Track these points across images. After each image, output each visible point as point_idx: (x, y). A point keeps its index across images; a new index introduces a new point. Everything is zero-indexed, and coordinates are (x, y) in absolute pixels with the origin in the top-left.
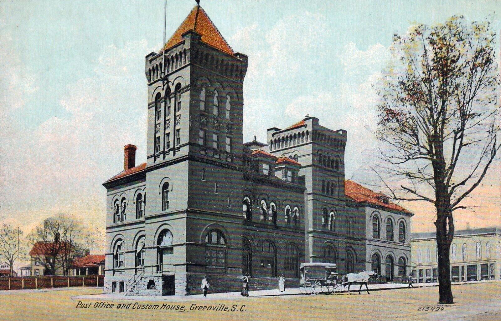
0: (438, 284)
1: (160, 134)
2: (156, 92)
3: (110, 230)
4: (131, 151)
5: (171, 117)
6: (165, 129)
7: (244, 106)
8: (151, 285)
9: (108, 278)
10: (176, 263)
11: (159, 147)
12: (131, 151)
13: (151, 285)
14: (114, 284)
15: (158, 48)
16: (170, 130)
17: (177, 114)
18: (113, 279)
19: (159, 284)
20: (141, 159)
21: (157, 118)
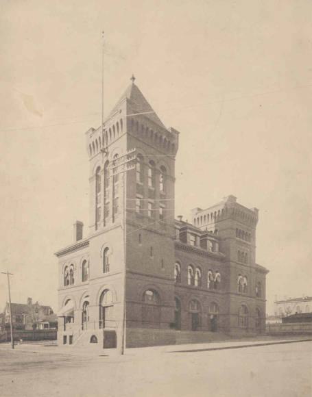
0: (267, 322)
1: (101, 205)
2: (97, 166)
3: (61, 292)
4: (79, 226)
5: (110, 188)
6: (105, 199)
7: (179, 157)
8: (93, 339)
9: (61, 333)
10: (117, 320)
11: (102, 215)
12: (79, 226)
13: (93, 339)
14: (65, 337)
15: (97, 124)
16: (110, 200)
17: (116, 184)
18: (65, 333)
19: (101, 338)
20: (87, 232)
21: (98, 190)
